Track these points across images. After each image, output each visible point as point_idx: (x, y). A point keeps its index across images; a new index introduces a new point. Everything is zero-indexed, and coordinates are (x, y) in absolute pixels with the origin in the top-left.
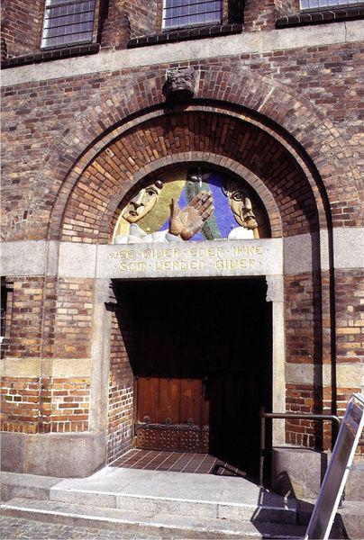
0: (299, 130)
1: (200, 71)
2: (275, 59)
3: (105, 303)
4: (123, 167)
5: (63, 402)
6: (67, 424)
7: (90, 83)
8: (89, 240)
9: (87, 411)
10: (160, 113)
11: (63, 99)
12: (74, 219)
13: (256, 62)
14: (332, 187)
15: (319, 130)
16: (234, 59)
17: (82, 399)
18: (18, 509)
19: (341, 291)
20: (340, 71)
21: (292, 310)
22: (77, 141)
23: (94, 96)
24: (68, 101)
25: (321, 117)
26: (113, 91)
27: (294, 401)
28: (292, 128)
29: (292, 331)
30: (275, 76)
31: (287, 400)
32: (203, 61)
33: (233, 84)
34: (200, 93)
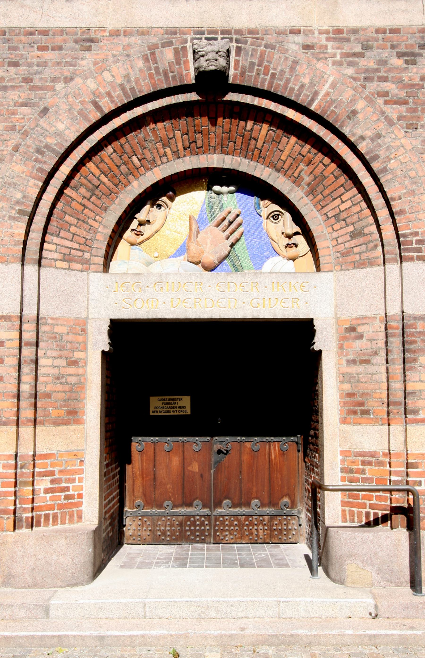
0: (363, 138)
1: (235, 44)
2: (334, 39)
3: (103, 352)
4: (123, 168)
5: (50, 486)
6: (55, 517)
7: (76, 41)
8: (78, 266)
9: (80, 496)
10: (193, 97)
11: (35, 61)
12: (58, 236)
13: (309, 41)
14: (402, 212)
15: (387, 140)
16: (280, 33)
17: (74, 480)
18: (14, 634)
19: (412, 339)
20: (414, 63)
21: (348, 361)
22: (61, 126)
23: (84, 63)
24: (45, 65)
25: (390, 123)
26: (111, 59)
27: (351, 471)
28: (354, 135)
29: (347, 387)
30: (334, 63)
31: (343, 470)
32: (238, 32)
33: (279, 68)
34: (235, 76)
